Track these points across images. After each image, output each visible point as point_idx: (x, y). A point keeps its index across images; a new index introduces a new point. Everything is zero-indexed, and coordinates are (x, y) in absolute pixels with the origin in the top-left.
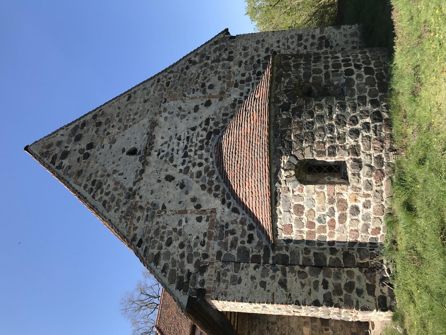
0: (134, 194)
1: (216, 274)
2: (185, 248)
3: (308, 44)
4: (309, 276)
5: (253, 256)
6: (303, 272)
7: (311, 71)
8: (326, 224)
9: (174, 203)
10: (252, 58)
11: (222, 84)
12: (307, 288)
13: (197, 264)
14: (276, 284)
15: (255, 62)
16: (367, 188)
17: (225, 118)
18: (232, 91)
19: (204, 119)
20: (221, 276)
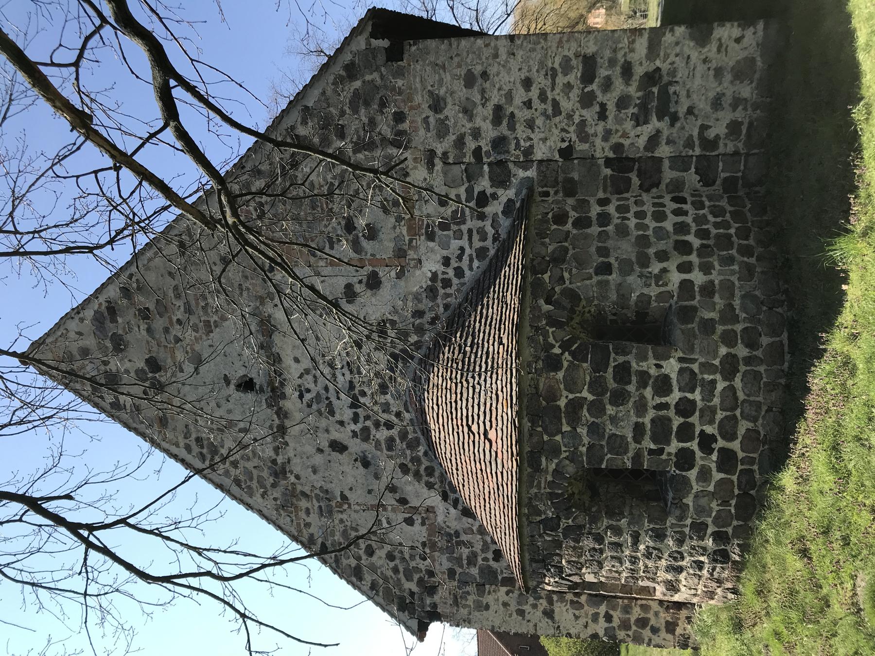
0: (284, 472)
1: (452, 597)
4: (586, 607)
5: (503, 578)
6: (577, 602)
7: (604, 443)
9: (359, 492)
11: (394, 227)
12: (582, 621)
13: (420, 582)
14: (539, 613)
15: (468, 157)
18: (422, 250)
20: (459, 600)
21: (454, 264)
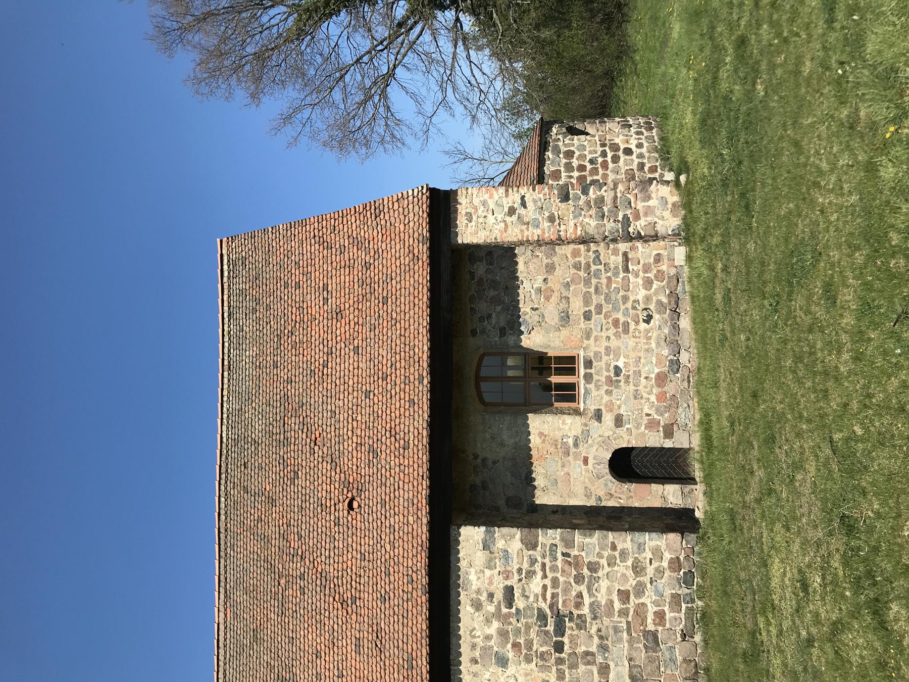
8: (599, 166)
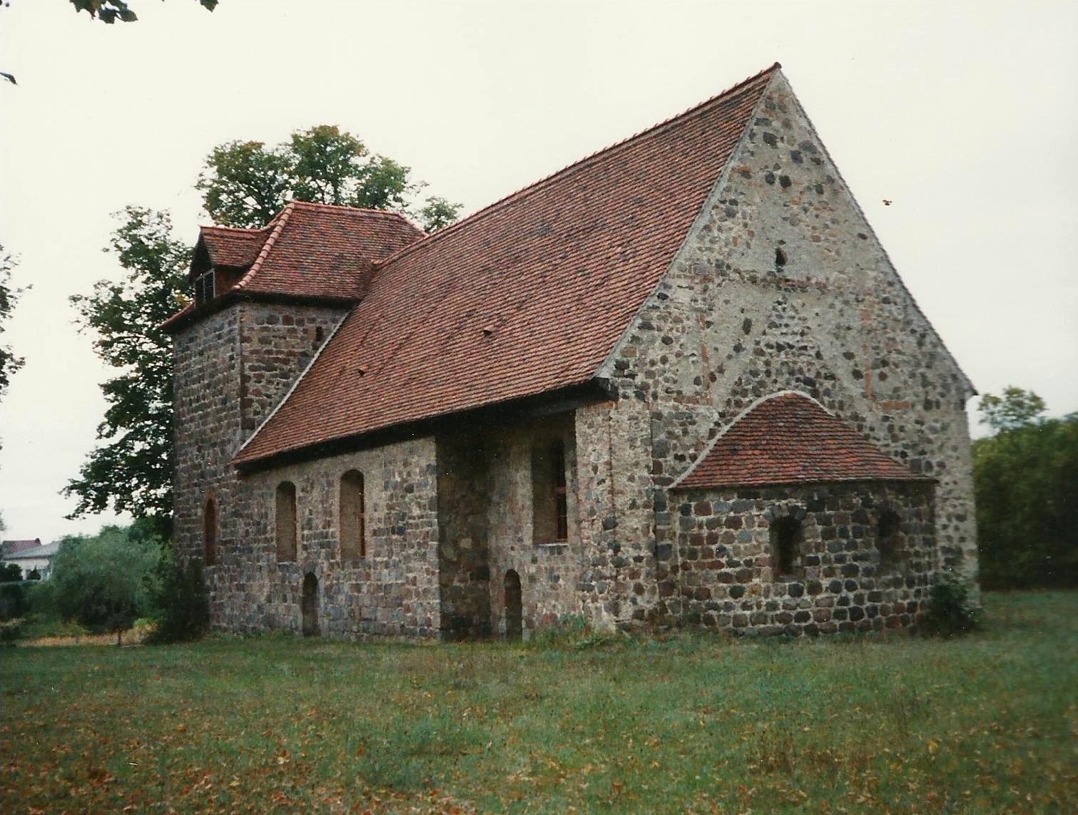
2: (662, 366)
3: (950, 531)
10: (930, 441)
16: (768, 604)
17: (837, 405)
19: (834, 371)
21: (871, 433)
